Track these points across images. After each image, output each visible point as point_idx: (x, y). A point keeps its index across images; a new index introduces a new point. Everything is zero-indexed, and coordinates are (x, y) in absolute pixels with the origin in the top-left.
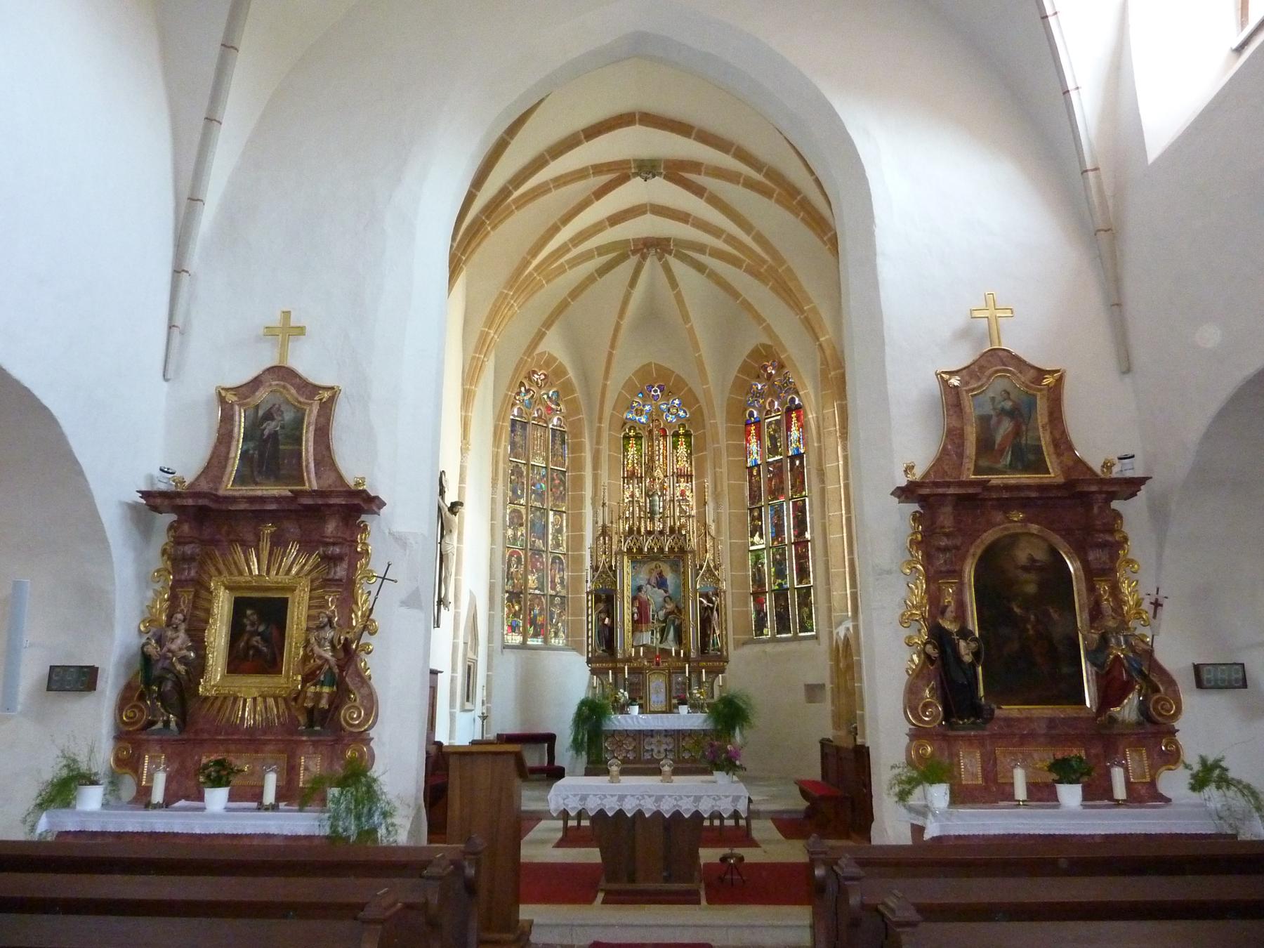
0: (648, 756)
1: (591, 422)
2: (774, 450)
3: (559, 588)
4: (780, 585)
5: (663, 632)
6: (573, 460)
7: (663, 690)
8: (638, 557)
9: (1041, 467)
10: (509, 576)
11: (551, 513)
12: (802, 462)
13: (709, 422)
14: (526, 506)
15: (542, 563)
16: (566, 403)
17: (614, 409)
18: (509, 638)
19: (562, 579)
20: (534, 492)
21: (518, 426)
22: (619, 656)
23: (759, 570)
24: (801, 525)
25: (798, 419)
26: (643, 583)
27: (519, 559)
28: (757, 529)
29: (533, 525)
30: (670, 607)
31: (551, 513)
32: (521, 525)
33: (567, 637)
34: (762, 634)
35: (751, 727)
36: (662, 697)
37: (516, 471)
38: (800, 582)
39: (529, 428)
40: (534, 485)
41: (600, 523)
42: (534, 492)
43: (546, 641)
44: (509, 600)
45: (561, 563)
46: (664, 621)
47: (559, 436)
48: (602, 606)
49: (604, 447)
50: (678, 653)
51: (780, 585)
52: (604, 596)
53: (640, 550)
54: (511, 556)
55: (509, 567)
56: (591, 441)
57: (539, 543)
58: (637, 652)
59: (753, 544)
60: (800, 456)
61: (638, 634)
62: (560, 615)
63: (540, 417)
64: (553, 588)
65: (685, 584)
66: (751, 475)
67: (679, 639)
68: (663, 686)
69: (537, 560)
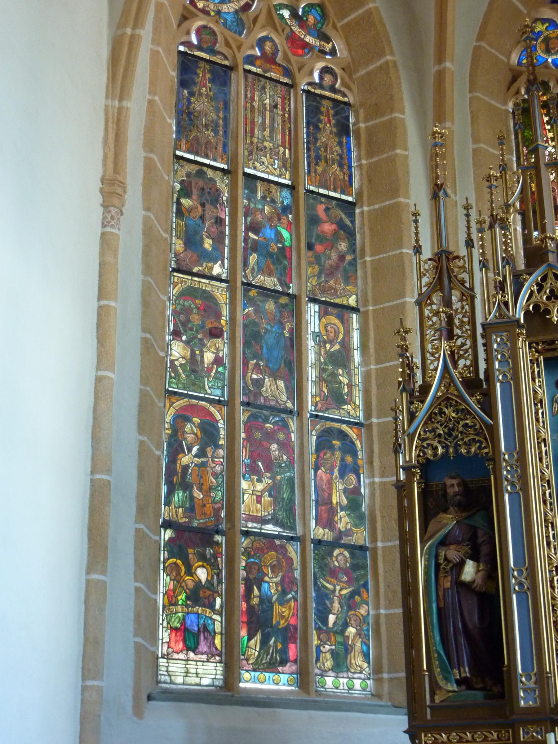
1: (418, 72)
3: (343, 521)
6: (372, 175)
10: (177, 479)
11: (312, 311)
14: (230, 282)
15: (285, 446)
16: (348, 33)
17: (481, 36)
18: (176, 667)
19: (354, 494)
20: (255, 247)
21: (203, 75)
27: (209, 434)
29: (253, 337)
31: (312, 310)
32: (216, 333)
33: (377, 670)
37: (197, 185)
39: (238, 84)
40: (254, 228)
42: (255, 247)
43: (304, 679)
44: (176, 548)
45: (349, 448)
47: (328, 113)
52: (453, 486)
54: (182, 418)
55: (176, 449)
57: (275, 389)
62: (350, 603)
63: (270, 59)
64: (327, 520)
69: (270, 436)
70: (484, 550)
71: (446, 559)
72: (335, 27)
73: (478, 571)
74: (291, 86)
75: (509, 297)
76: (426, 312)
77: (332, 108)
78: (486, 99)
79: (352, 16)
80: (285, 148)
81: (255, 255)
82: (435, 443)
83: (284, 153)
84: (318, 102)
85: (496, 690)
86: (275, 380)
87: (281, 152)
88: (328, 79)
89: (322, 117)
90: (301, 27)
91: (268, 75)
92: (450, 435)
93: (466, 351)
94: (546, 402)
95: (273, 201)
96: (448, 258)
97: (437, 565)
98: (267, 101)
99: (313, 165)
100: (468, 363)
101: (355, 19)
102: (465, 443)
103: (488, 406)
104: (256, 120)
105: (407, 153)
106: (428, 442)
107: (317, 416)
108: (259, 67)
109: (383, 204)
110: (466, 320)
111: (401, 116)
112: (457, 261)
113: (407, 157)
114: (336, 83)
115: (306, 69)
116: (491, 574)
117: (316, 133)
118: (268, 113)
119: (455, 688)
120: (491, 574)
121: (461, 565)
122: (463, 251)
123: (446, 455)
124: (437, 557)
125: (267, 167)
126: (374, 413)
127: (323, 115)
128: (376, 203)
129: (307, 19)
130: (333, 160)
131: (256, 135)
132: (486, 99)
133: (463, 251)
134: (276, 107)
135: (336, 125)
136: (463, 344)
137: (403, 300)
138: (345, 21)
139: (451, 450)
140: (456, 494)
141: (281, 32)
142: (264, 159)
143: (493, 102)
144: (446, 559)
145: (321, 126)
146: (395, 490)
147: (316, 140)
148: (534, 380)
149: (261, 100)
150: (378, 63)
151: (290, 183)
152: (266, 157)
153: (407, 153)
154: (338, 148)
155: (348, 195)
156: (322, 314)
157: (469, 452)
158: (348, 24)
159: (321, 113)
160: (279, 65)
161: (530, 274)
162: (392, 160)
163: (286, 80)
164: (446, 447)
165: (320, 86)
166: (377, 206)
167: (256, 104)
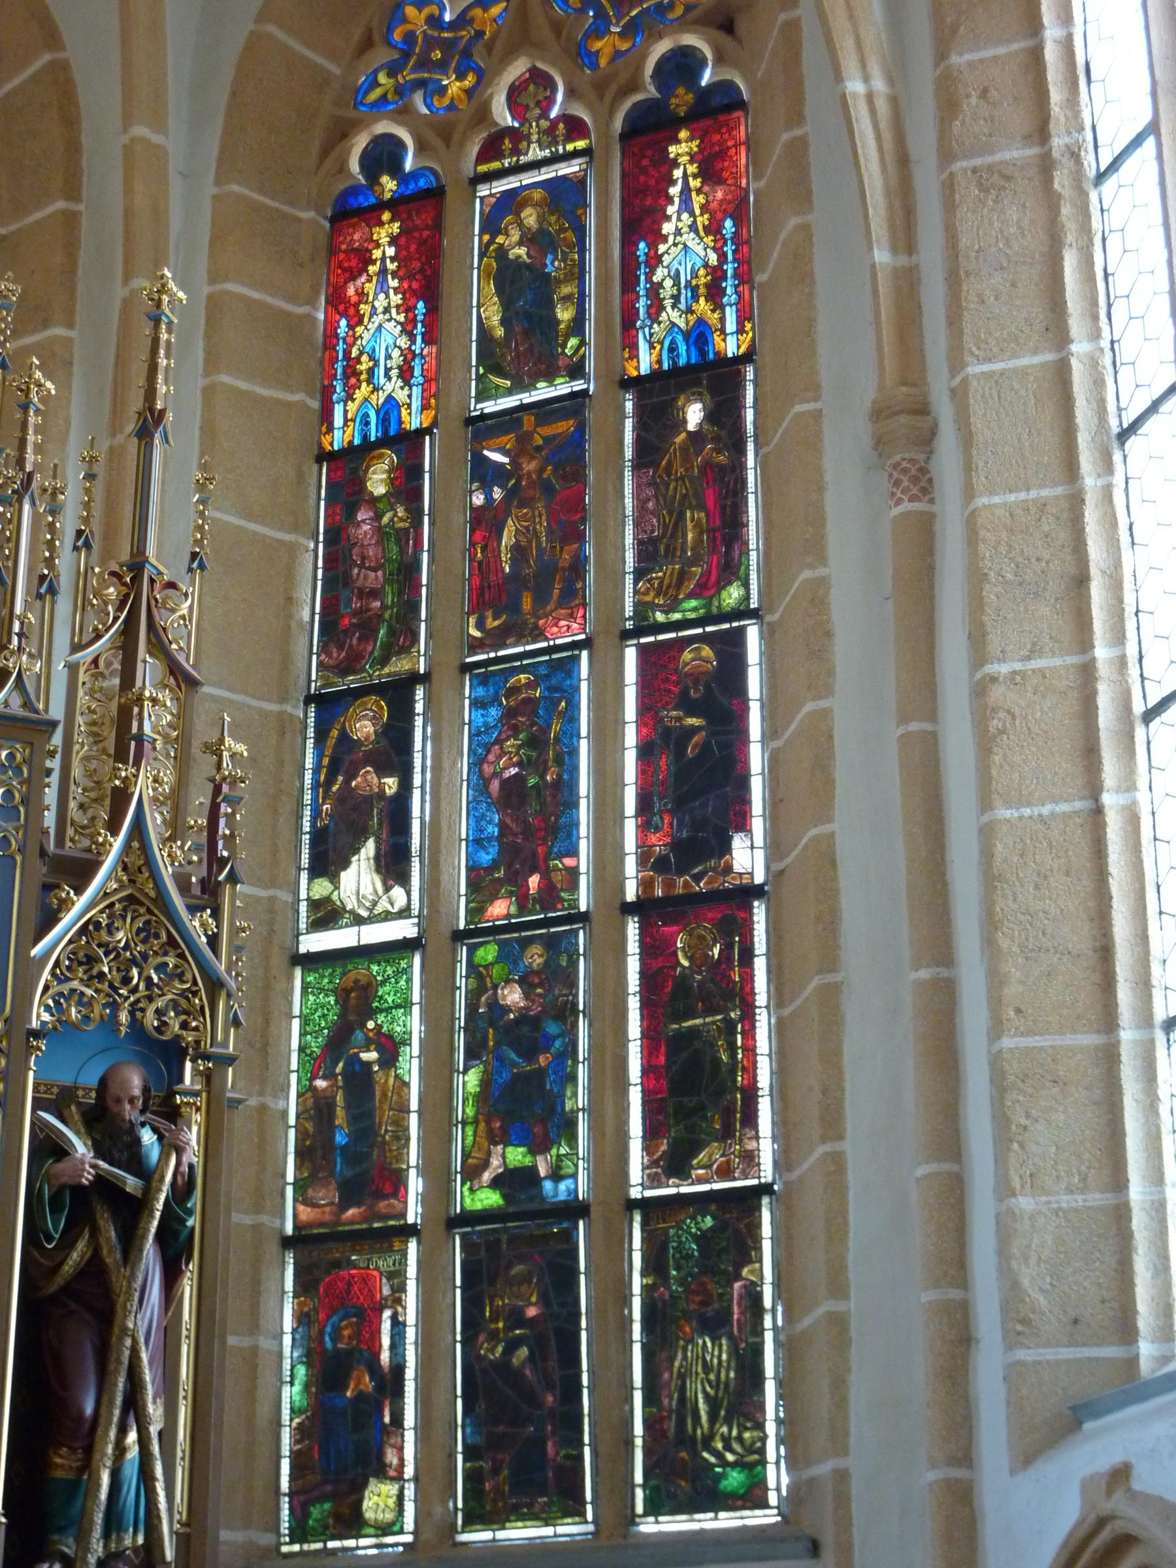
2: (529, 341)
4: (516, 1182)
12: (724, 414)
23: (360, 1082)
24: (697, 786)
25: (711, 167)
28: (360, 821)
34: (351, 1521)
38: (674, 1164)
51: (516, 1182)
59: (327, 915)
60: (718, 378)
66: (347, 492)
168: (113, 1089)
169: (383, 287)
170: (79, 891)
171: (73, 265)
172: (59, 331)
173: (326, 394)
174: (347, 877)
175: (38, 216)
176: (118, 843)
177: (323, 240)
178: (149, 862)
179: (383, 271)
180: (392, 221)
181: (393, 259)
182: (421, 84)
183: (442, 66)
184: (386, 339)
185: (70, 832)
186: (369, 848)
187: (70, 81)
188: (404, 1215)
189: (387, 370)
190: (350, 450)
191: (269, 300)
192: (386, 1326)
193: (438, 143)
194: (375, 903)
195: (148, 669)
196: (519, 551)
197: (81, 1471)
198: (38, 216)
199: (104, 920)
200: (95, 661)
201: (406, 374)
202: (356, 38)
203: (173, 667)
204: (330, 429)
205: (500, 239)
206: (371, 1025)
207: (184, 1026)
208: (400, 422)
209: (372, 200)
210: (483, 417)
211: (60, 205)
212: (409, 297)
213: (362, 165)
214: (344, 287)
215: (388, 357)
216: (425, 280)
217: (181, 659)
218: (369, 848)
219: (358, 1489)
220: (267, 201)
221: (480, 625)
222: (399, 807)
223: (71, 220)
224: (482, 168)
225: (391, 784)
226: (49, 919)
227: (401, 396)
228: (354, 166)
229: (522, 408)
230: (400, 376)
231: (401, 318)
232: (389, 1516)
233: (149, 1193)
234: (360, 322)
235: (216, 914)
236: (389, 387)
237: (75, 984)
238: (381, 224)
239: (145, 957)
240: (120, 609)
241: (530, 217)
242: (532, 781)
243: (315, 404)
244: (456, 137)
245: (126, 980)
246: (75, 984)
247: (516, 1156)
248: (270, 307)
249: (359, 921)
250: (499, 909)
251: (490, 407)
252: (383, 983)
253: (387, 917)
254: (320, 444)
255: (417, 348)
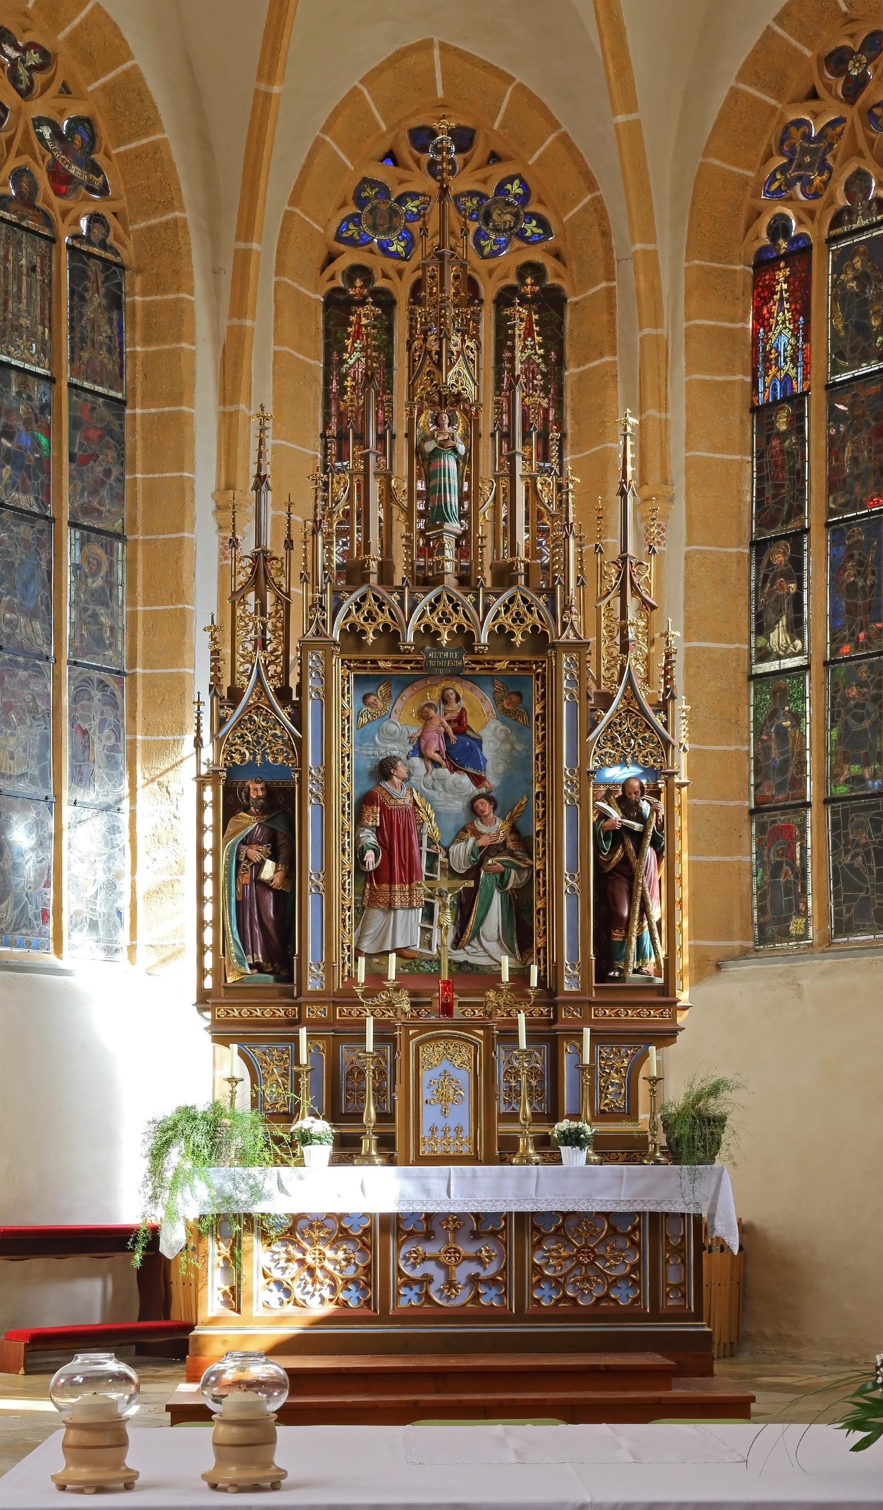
0: (409, 1298)
1: (213, 237)
5: (464, 908)
7: (466, 1094)
8: (384, 665)
9: (430, 948)
13: (628, 245)
17: (294, 200)
22: (313, 984)
26: (397, 749)
30: (494, 829)
31: (69, 538)
35: (206, 1029)
36: (461, 1114)
41: (248, 546)
46: (473, 873)
48: (249, 822)
49: (261, 322)
50: (520, 976)
52: (256, 791)
53: (390, 637)
56: (215, 293)
58: (376, 977)
61: (377, 917)
65: (548, 757)
67: (521, 933)
68: (464, 1077)
70: (283, 854)
71: (246, 858)
72: (107, 154)
73: (276, 871)
74: (52, 240)
75: (328, 616)
76: (239, 612)
77: (102, 272)
78: (295, 285)
79: (133, 145)
80: (44, 327)
81: (8, 467)
82: (244, 750)
83: (43, 333)
84: (85, 263)
85: (283, 973)
86: (31, 621)
87: (40, 332)
88: (98, 232)
89: (89, 285)
90: (66, 152)
91: (24, 224)
92: (258, 743)
93: (277, 657)
94: (353, 718)
95: (30, 398)
96: (265, 558)
97: (238, 863)
98: (24, 262)
99: (76, 350)
100: (279, 669)
101: (136, 148)
102: (273, 752)
103: (298, 720)
104: (10, 288)
105: (194, 348)
106: (237, 747)
107: (75, 663)
108: (14, 213)
109: (162, 410)
110: (279, 625)
111: (188, 297)
112: (274, 562)
113: (193, 353)
114: (107, 237)
115: (70, 217)
116: (289, 876)
117: (82, 306)
118: (24, 277)
119: (249, 971)
120: (289, 876)
121: (260, 866)
122: (281, 553)
123: (252, 763)
124: (238, 854)
125: (23, 353)
126: (140, 661)
127: (89, 281)
128: (152, 406)
129: (73, 141)
130: (101, 344)
131: (10, 309)
132: (295, 285)
133: (281, 553)
134: (33, 269)
135: (106, 296)
136: (275, 650)
137: (181, 535)
138: (122, 149)
139: (258, 757)
140: (259, 798)
141: (41, 162)
142: (19, 342)
143: (302, 289)
144: (246, 858)
145: (87, 296)
146: (195, 784)
147: (82, 315)
148: (343, 696)
149: (17, 260)
150: (164, 219)
151: (48, 373)
152: (21, 338)
153: (194, 348)
154: (107, 327)
155: (118, 391)
156: (84, 542)
157: (275, 761)
158: (126, 154)
159: (87, 278)
160: (38, 209)
161: (351, 593)
162: (176, 354)
163: (46, 233)
164: (254, 754)
165: (88, 240)
166: (153, 410)
167: (10, 266)
168: (628, 790)
169: (781, 309)
170: (606, 711)
171: (612, 322)
172: (608, 359)
173: (755, 372)
174: (773, 636)
175: (593, 291)
176: (621, 689)
177: (750, 280)
178: (635, 696)
179: (781, 299)
180: (786, 267)
181: (786, 291)
182: (799, 178)
183: (810, 167)
184: (784, 340)
185: (603, 681)
186: (784, 621)
187: (603, 208)
188: (805, 797)
189: (785, 358)
190: (767, 405)
191: (720, 324)
192: (798, 849)
193: (806, 219)
194: (787, 648)
195: (632, 603)
196: (855, 460)
197: (625, 937)
198: (593, 291)
199: (617, 721)
200: (609, 603)
201: (794, 360)
202: (762, 153)
203: (644, 602)
204: (757, 393)
205: (842, 277)
206: (787, 708)
207: (655, 761)
208: (792, 388)
209: (775, 254)
210: (835, 384)
211: (604, 284)
212: (795, 312)
213: (768, 234)
214: (762, 309)
215: (785, 350)
216: (802, 307)
217: (647, 597)
218: (784, 621)
219: (788, 919)
220: (715, 265)
221: (834, 502)
222: (797, 600)
223: (610, 291)
224: (833, 233)
225: (793, 586)
226: (595, 725)
227: (792, 373)
228: (764, 235)
229: (854, 378)
230: (791, 361)
231: (791, 327)
232: (801, 932)
233: (645, 829)
234: (770, 330)
235: (666, 713)
236: (786, 368)
237: (607, 750)
238: (780, 269)
239: (636, 734)
240: (617, 579)
241: (858, 263)
242: (860, 584)
243: (749, 379)
244: (817, 215)
245: (629, 745)
246: (607, 750)
247: (855, 769)
248: (721, 328)
249: (779, 657)
250: (846, 650)
251: (839, 378)
252: (792, 688)
253: (794, 655)
254: (752, 401)
255: (800, 345)
